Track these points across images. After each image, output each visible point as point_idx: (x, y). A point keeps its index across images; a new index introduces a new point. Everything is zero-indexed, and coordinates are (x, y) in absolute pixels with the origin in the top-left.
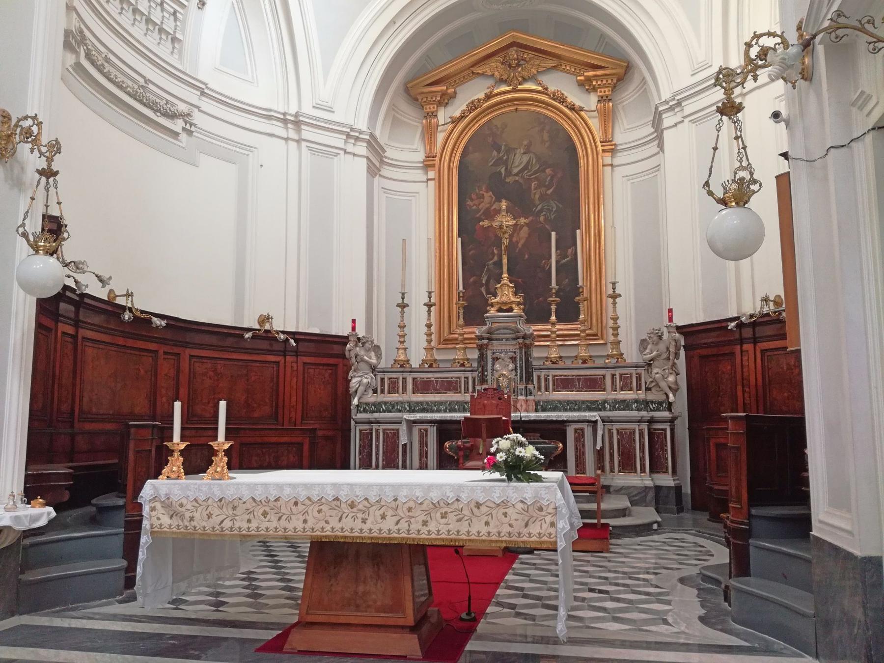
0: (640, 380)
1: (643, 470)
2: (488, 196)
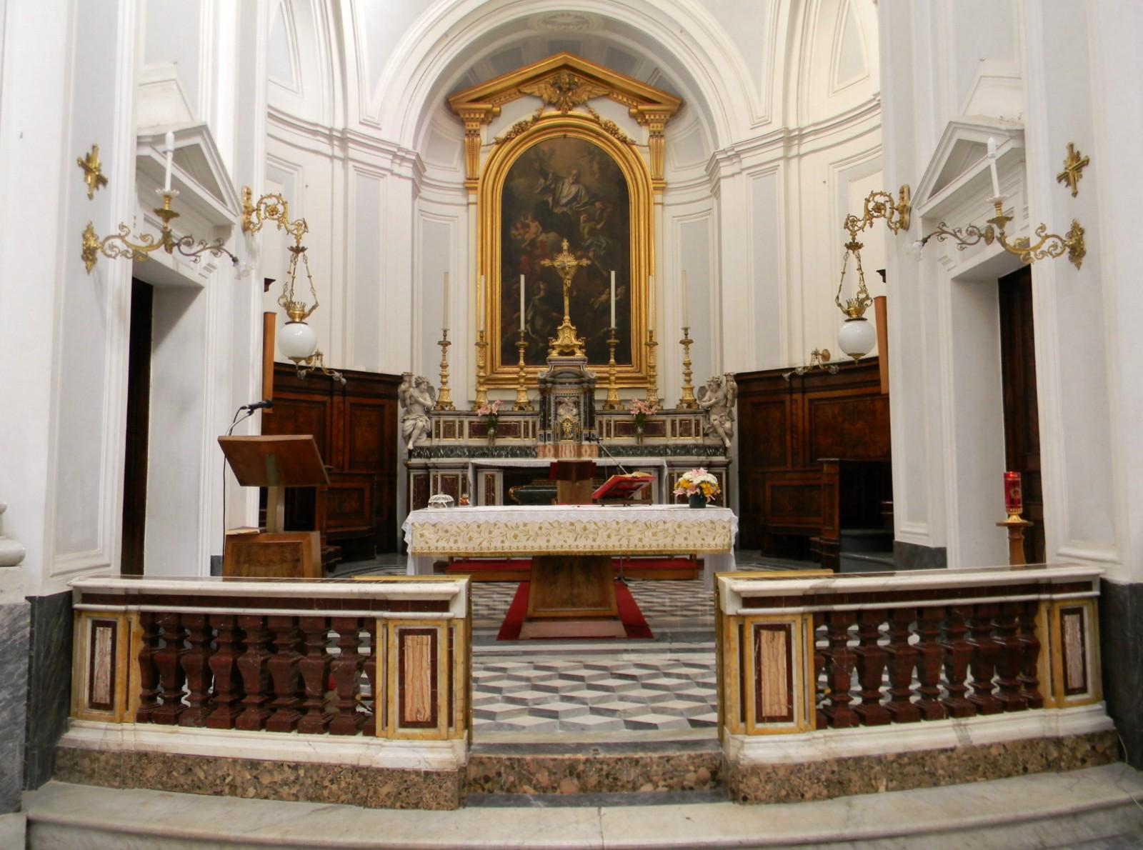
0: (699, 426)
2: (534, 226)
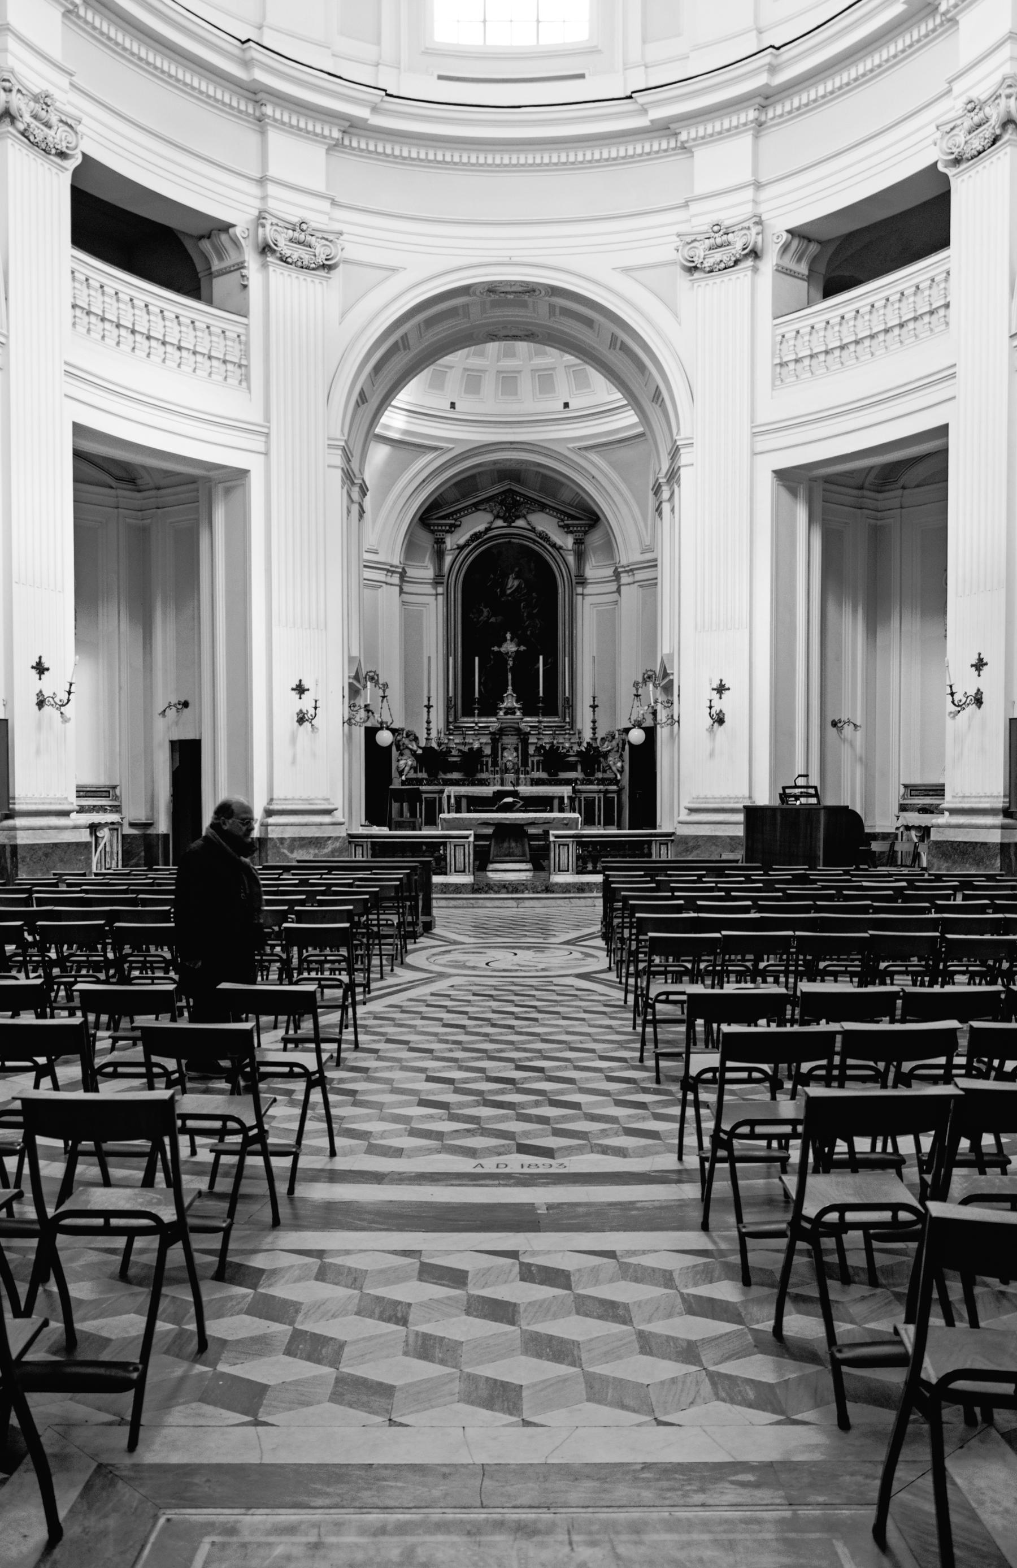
1: (599, 824)
